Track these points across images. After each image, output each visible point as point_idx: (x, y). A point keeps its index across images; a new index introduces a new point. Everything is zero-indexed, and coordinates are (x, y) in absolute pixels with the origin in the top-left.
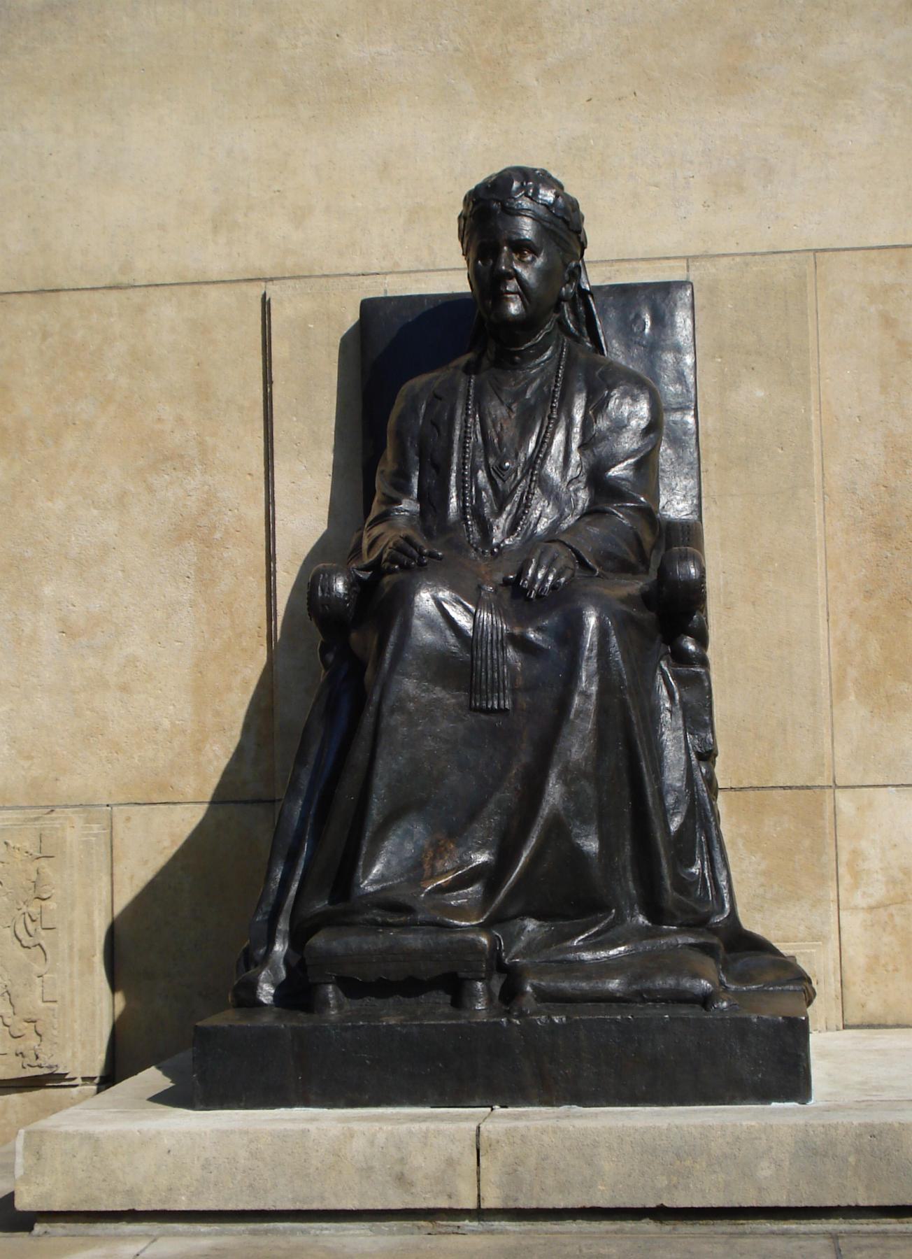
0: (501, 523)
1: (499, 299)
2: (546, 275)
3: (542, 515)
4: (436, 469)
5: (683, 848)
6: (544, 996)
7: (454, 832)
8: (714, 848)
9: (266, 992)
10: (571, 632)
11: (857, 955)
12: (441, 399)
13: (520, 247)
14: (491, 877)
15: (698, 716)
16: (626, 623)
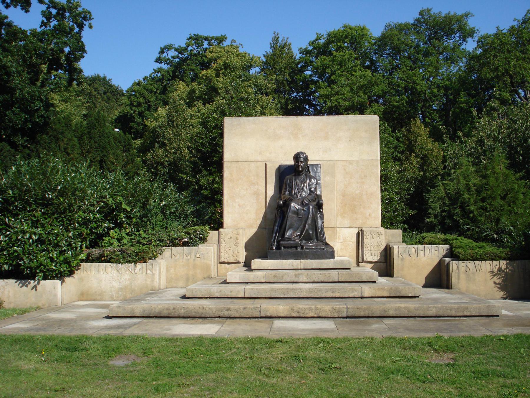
0: (299, 195)
1: (299, 168)
2: (304, 165)
3: (304, 194)
4: (291, 188)
5: (320, 233)
6: (306, 248)
7: (295, 231)
8: (324, 233)
9: (274, 248)
10: (309, 209)
11: (339, 248)
12: (291, 180)
13: (301, 162)
14: (300, 236)
15: (322, 218)
16: (315, 207)
